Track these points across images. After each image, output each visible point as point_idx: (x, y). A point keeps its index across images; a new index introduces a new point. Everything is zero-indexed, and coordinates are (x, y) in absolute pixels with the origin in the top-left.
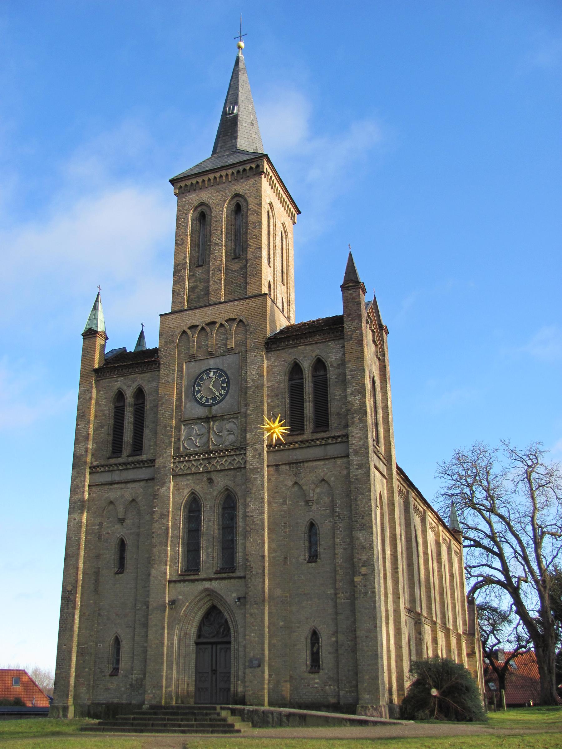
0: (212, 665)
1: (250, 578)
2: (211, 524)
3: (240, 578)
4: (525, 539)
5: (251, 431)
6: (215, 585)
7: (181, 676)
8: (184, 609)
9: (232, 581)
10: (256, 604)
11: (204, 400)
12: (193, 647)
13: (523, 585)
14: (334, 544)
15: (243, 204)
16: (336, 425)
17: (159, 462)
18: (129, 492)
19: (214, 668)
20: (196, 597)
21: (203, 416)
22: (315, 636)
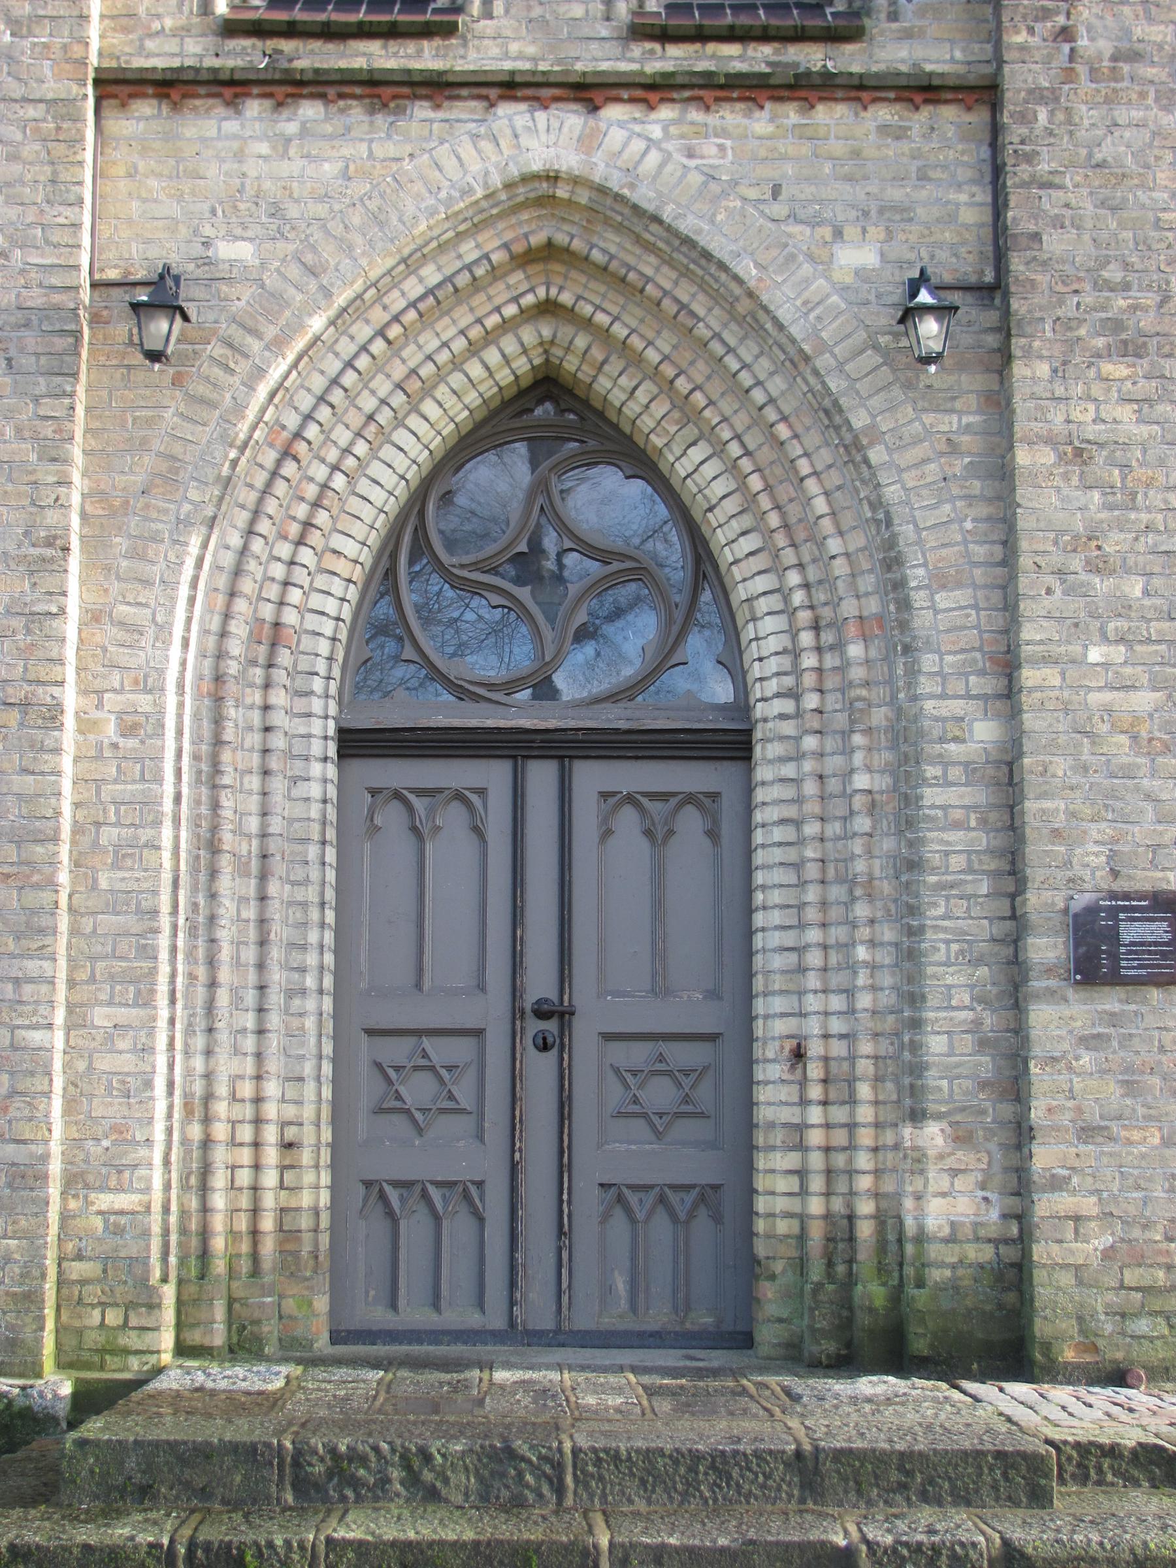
1: (1049, 97)
3: (922, 90)
6: (633, 148)
7: (226, 1065)
8: (275, 373)
9: (831, 116)
19: (540, 983)
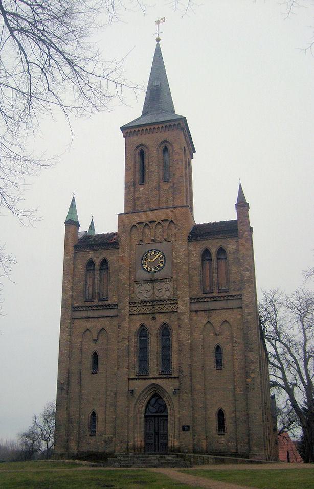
0: (155, 430)
2: (154, 344)
4: (298, 357)
5: (181, 290)
6: (158, 382)
10: (186, 393)
11: (149, 269)
12: (143, 419)
13: (295, 388)
14: (233, 359)
15: (170, 148)
16: (233, 288)
17: (120, 305)
18: (99, 324)
20: (146, 388)
21: (148, 279)
22: (221, 414)
